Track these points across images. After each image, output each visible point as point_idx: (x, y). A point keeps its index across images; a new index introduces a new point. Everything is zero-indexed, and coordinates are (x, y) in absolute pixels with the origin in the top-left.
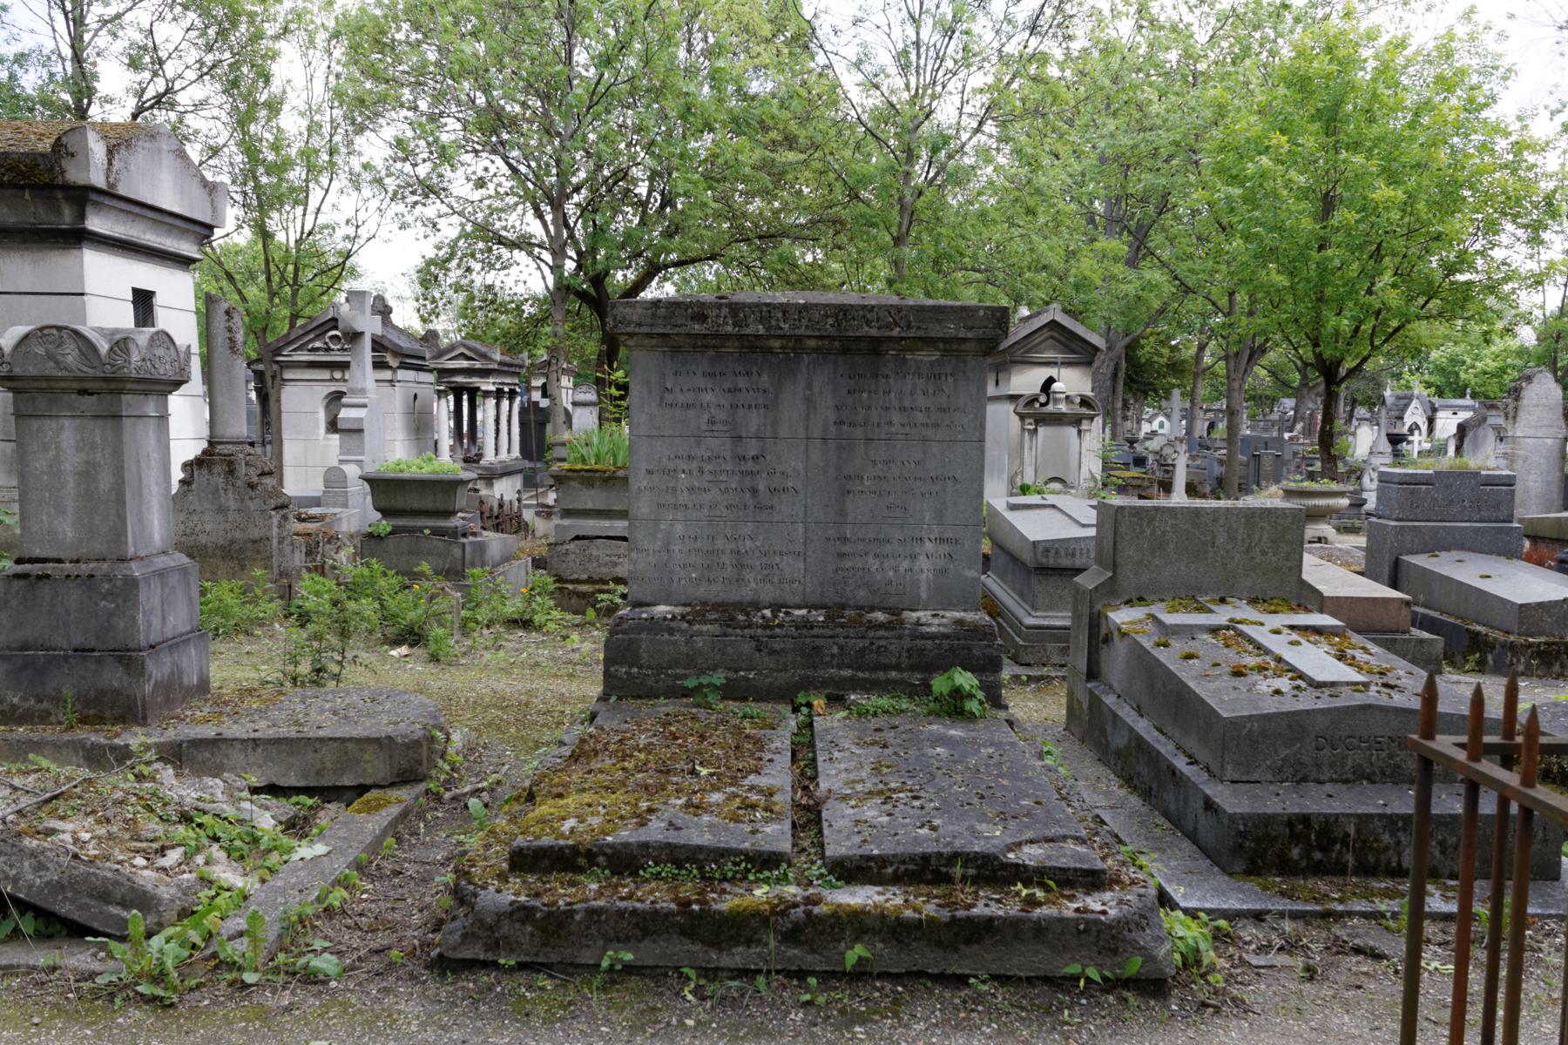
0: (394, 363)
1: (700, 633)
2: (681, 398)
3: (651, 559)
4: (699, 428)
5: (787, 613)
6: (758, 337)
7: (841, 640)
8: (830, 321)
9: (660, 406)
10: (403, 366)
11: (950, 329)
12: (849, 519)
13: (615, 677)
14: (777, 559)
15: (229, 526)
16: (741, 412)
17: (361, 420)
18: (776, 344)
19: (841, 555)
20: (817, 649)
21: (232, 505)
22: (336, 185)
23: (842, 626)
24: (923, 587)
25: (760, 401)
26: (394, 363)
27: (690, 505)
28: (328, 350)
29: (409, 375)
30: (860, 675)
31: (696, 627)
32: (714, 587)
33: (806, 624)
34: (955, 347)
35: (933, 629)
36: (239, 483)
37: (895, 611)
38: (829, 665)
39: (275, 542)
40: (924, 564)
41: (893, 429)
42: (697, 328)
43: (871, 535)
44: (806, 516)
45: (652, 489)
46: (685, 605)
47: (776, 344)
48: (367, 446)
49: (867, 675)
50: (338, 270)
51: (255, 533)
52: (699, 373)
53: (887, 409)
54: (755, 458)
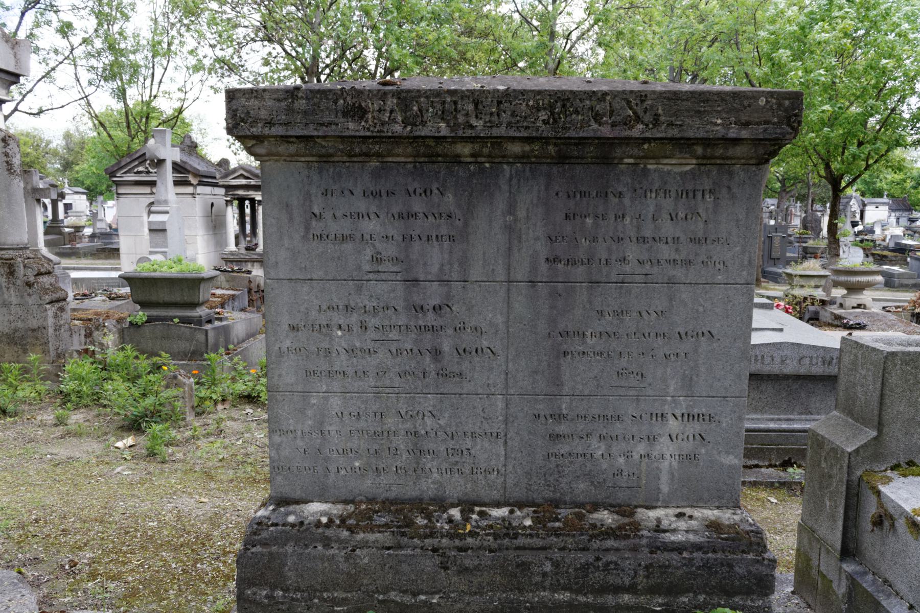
0: (194, 181)
1: (365, 545)
2: (335, 228)
3: (300, 443)
4: (359, 268)
5: (482, 514)
6: (439, 139)
7: (557, 555)
8: (543, 115)
9: (304, 238)
10: (201, 183)
11: (717, 126)
12: (566, 390)
13: (254, 602)
14: (469, 442)
15: (12, 318)
16: (417, 246)
17: (164, 223)
18: (465, 150)
19: (556, 437)
20: (524, 566)
21: (14, 300)
22: (171, 64)
23: (556, 533)
24: (664, 478)
25: (444, 231)
26: (194, 181)
27: (350, 371)
28: (148, 172)
29: (208, 190)
30: (582, 599)
31: (361, 536)
32: (384, 480)
33: (508, 530)
34: (720, 151)
35: (679, 537)
36: (19, 282)
37: (625, 510)
38: (540, 586)
39: (51, 331)
40: (665, 447)
41: (628, 269)
42: (352, 127)
43: (595, 411)
44: (507, 386)
45: (298, 350)
46: (346, 502)
47: (465, 150)
48: (169, 241)
49: (590, 599)
50: (174, 120)
51: (34, 323)
52: (358, 191)
53: (620, 239)
54: (437, 309)
